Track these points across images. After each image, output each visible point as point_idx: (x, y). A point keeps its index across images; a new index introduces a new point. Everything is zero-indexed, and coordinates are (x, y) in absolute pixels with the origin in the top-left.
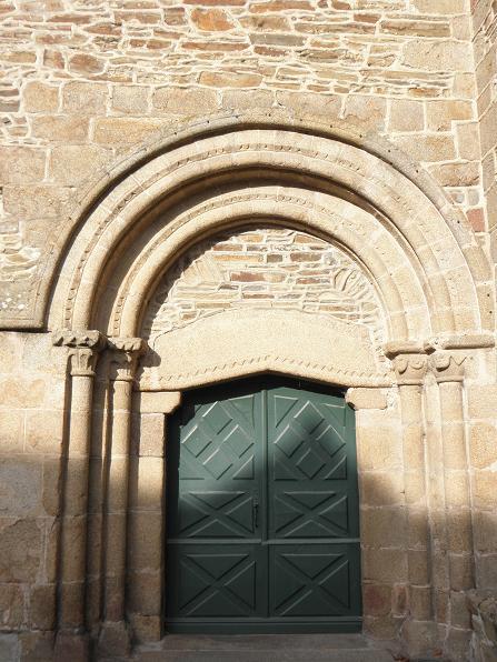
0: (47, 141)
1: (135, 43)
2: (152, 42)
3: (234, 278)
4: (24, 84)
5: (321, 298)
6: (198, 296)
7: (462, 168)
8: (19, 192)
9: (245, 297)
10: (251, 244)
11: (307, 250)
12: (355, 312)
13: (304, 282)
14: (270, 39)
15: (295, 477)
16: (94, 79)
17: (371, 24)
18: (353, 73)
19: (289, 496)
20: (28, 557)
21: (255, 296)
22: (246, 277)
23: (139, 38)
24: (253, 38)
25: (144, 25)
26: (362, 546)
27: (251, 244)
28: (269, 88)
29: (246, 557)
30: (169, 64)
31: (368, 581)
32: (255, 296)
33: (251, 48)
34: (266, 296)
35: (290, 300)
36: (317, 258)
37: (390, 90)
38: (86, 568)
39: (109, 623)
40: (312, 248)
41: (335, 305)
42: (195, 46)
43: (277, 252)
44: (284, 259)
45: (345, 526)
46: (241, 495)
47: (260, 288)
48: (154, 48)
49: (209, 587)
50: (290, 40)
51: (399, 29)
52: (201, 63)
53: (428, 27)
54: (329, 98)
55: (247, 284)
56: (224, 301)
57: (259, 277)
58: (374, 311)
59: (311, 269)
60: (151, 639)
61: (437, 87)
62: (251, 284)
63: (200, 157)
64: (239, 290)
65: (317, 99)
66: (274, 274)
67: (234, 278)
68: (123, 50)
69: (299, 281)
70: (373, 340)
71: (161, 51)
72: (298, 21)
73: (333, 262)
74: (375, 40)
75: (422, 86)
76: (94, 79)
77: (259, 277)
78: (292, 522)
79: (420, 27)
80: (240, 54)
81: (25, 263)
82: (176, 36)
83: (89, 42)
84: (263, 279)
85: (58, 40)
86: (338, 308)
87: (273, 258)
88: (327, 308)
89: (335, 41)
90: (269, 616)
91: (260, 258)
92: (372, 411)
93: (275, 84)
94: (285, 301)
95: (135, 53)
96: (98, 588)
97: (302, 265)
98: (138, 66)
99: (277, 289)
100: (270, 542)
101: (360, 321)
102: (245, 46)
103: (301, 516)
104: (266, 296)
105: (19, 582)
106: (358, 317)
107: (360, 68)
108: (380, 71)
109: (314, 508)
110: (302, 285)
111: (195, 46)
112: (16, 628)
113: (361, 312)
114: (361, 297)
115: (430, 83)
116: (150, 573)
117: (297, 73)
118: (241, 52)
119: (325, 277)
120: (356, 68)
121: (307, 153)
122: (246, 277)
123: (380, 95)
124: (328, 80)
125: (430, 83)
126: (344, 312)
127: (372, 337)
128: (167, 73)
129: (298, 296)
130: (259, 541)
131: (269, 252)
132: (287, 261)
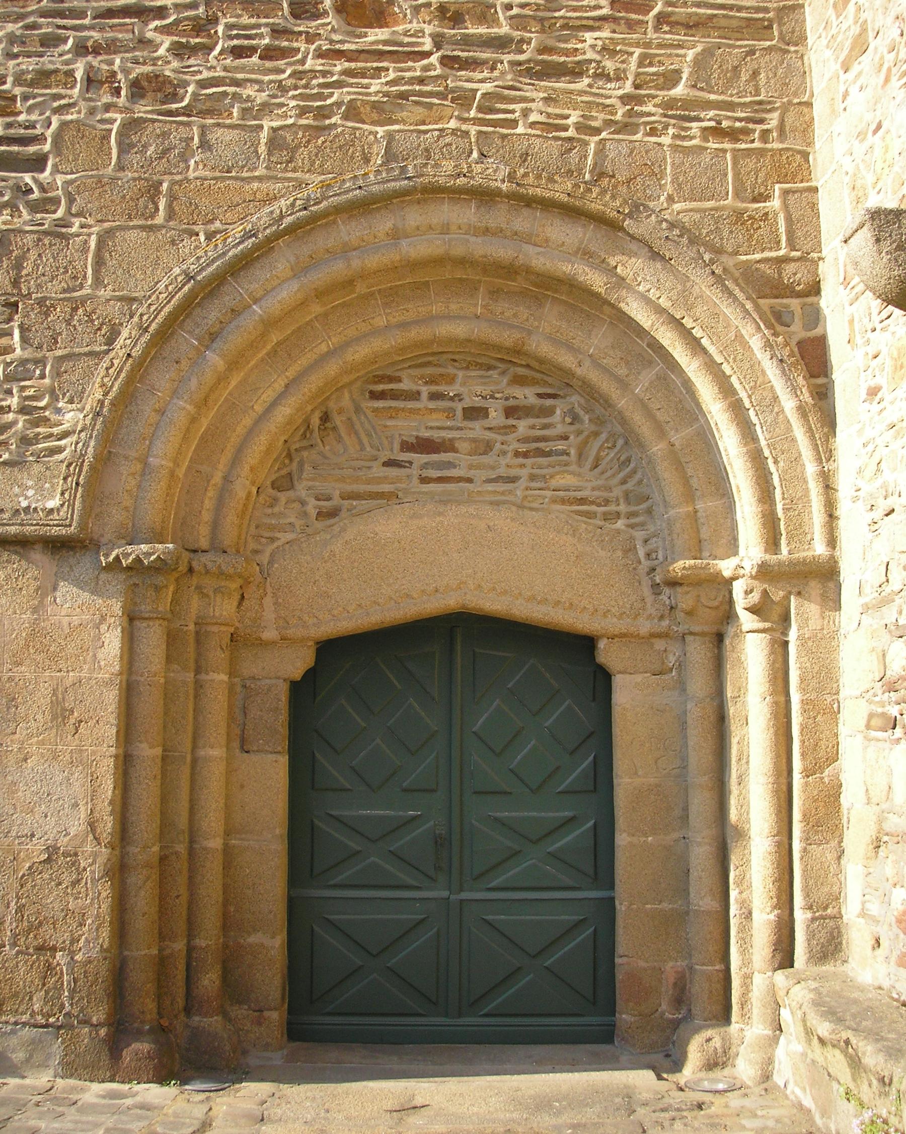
0: (90, 221)
1: (238, 52)
2: (267, 48)
3: (407, 447)
4: (55, 125)
5: (554, 483)
6: (342, 479)
7: (790, 268)
8: (45, 307)
9: (424, 480)
10: (434, 388)
11: (533, 400)
12: (612, 508)
13: (525, 455)
14: (467, 42)
15: (508, 790)
16: (170, 113)
17: (640, 17)
18: (608, 102)
19: (496, 819)
20: (66, 911)
21: (440, 480)
22: (425, 446)
23: (246, 42)
24: (438, 41)
25: (253, 21)
26: (617, 902)
27: (434, 388)
28: (464, 127)
29: (424, 919)
30: (296, 88)
31: (625, 960)
32: (440, 480)
33: (434, 59)
34: (460, 479)
35: (501, 487)
36: (550, 412)
37: (671, 131)
38: (166, 826)
39: (197, 1018)
40: (540, 396)
41: (579, 494)
42: (340, 54)
43: (477, 402)
44: (492, 414)
45: (591, 872)
46: (414, 818)
47: (450, 465)
48: (270, 58)
49: (519, 969)
50: (501, 43)
51: (688, 27)
52: (351, 85)
53: (735, 23)
54: (567, 145)
55: (424, 458)
56: (386, 488)
57: (447, 446)
58: (644, 506)
59: (539, 433)
60: (267, 1047)
61: (751, 126)
62: (435, 457)
63: (346, 249)
64: (415, 472)
65: (547, 150)
66: (474, 440)
67: (407, 447)
68: (215, 63)
69: (517, 454)
70: (641, 553)
71: (281, 63)
72: (515, 11)
73: (575, 419)
74: (648, 45)
75: (725, 124)
76: (170, 113)
77: (447, 446)
78: (500, 864)
79: (723, 22)
80: (416, 68)
81: (56, 430)
82: (310, 38)
83: (162, 51)
84: (454, 450)
85: (112, 47)
86: (582, 501)
87: (474, 413)
88: (563, 501)
89: (579, 46)
90: (460, 1015)
91: (450, 413)
92: (639, 678)
93: (476, 121)
94: (490, 487)
95: (237, 69)
96: (182, 966)
97: (522, 426)
98: (249, 91)
99: (478, 467)
100: (464, 895)
101: (620, 524)
102: (428, 54)
103: (517, 853)
104: (460, 479)
105: (54, 949)
106: (618, 515)
107: (621, 92)
108: (654, 97)
109: (540, 840)
110: (521, 460)
111: (340, 54)
112: (51, 1020)
113: (622, 508)
114: (624, 482)
115: (740, 120)
116: (270, 943)
117: (513, 100)
118: (419, 65)
119: (560, 446)
120: (614, 91)
121: (528, 239)
122: (425, 446)
123: (653, 139)
124: (566, 112)
125: (740, 120)
126: (593, 508)
127: (641, 553)
128: (293, 103)
129: (513, 480)
130: (445, 894)
131: (467, 403)
132: (496, 416)
